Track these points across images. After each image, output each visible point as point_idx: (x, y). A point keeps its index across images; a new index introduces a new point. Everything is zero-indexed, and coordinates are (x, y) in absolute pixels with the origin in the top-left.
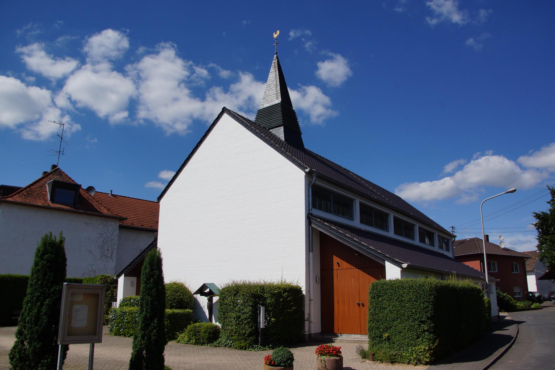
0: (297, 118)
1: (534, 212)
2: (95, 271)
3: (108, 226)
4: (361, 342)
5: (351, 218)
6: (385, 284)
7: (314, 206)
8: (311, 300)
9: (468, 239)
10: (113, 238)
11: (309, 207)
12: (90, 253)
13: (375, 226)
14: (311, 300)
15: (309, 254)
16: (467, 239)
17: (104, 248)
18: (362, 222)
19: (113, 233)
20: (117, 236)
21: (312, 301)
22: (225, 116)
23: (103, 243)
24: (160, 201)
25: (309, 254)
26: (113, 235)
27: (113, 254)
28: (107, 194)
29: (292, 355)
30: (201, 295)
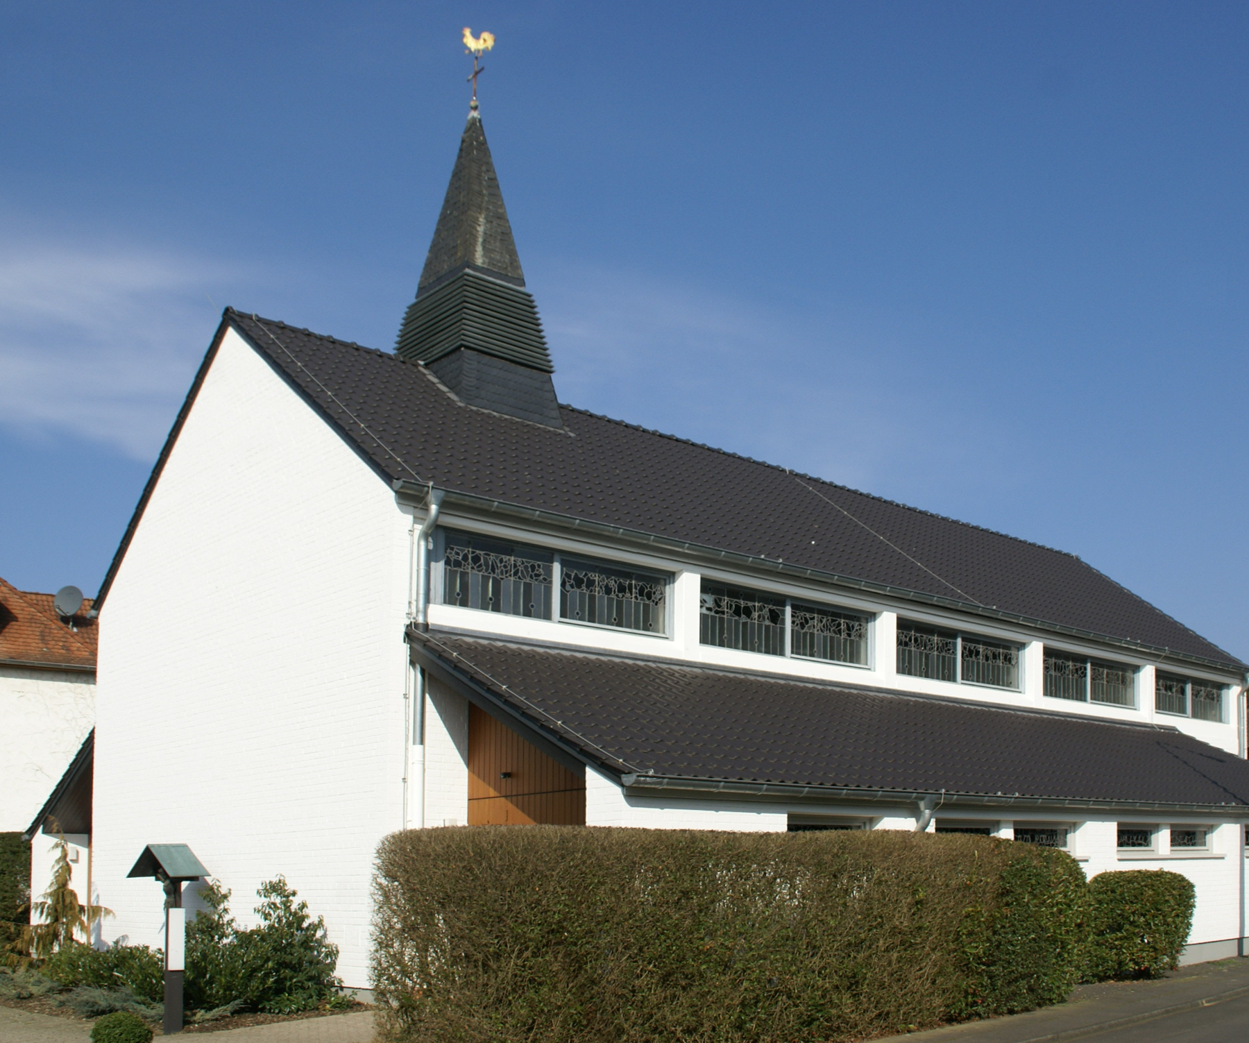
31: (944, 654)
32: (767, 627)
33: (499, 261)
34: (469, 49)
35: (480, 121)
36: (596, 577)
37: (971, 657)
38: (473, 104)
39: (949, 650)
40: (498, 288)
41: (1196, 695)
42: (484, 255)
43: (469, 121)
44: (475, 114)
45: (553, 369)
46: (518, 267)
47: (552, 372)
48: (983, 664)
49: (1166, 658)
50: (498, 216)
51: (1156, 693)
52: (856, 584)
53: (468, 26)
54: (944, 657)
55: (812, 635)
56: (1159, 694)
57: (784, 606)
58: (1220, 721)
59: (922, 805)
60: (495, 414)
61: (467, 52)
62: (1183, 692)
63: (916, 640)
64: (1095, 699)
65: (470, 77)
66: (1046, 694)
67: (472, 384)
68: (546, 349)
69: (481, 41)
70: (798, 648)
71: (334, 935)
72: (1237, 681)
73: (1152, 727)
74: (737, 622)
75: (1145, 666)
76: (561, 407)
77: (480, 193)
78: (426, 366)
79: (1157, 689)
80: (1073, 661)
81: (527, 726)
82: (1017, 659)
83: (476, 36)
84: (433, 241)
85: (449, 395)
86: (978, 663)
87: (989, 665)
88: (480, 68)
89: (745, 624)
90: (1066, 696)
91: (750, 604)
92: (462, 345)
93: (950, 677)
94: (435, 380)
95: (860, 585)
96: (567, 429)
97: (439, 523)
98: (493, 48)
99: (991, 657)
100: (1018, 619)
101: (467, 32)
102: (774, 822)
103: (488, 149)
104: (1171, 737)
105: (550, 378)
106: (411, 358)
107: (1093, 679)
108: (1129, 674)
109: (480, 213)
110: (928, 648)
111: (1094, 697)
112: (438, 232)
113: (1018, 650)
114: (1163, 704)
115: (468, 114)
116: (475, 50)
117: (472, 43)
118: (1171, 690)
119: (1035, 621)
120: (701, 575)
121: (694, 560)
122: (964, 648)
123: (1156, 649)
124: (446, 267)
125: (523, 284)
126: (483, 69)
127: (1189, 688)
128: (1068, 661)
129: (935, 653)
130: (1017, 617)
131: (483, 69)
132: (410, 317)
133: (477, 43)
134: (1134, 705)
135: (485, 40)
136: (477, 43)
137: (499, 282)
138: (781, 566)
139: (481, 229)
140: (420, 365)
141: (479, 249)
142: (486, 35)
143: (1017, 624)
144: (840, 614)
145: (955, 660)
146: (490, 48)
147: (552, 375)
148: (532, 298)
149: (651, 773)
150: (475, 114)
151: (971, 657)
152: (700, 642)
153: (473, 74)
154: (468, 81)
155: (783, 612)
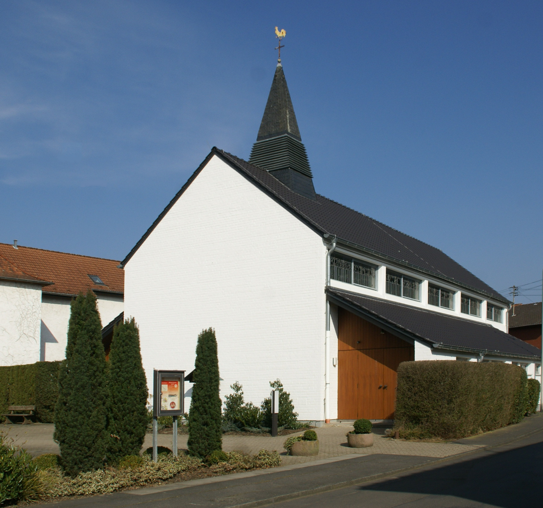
0: (307, 155)
1: (286, 389)
2: (13, 357)
3: (27, 294)
4: (341, 240)
5: (375, 288)
6: (414, 363)
7: (332, 277)
8: (327, 384)
9: (536, 303)
10: (34, 310)
11: (327, 279)
12: (4, 331)
13: (404, 295)
14: (327, 384)
15: (326, 332)
16: (534, 304)
17: (23, 325)
18: (388, 291)
19: (33, 303)
20: (40, 308)
21: (328, 385)
22: (215, 158)
23: (21, 317)
24: (124, 266)
25: (326, 332)
26: (34, 307)
27: (36, 332)
28: (10, 245)
29: (314, 432)
30: (190, 382)
31: (346, 269)
32: (398, 285)
34: (277, 36)
35: (282, 68)
36: (361, 267)
37: (357, 271)
39: (349, 267)
40: (296, 142)
41: (356, 270)
42: (290, 128)
43: (277, 67)
44: (279, 65)
45: (312, 176)
46: (299, 133)
47: (312, 177)
48: (362, 275)
49: (491, 298)
50: (292, 112)
51: (386, 282)
52: (410, 266)
53: (277, 26)
54: (347, 271)
55: (407, 288)
56: (388, 283)
57: (401, 278)
58: (501, 323)
59: (481, 354)
61: (277, 37)
62: (399, 282)
63: (336, 261)
64: (356, 283)
65: (277, 48)
66: (429, 303)
70: (464, 310)
71: (539, 381)
72: (506, 307)
73: (484, 324)
74: (391, 284)
75: (484, 300)
79: (387, 280)
80: (436, 289)
81: (379, 322)
82: (375, 273)
83: (280, 31)
84: (264, 117)
86: (360, 275)
87: (364, 276)
89: (393, 284)
90: (394, 294)
91: (394, 277)
93: (349, 282)
94: (272, 176)
95: (411, 266)
97: (335, 250)
98: (286, 36)
99: (365, 272)
100: (417, 268)
101: (277, 28)
102: (454, 358)
103: (286, 81)
104: (491, 328)
106: (261, 166)
107: (471, 305)
108: (417, 284)
110: (340, 266)
111: (356, 282)
113: (501, 310)
114: (390, 290)
115: (277, 65)
117: (277, 32)
118: (393, 281)
119: (385, 256)
120: (386, 267)
121: (461, 287)
122: (354, 267)
123: (382, 255)
124: (274, 130)
125: (301, 140)
126: (284, 46)
127: (493, 309)
128: (434, 288)
129: (343, 268)
130: (417, 267)
131: (284, 46)
133: (281, 34)
134: (453, 309)
136: (281, 34)
137: (295, 139)
138: (407, 264)
139: (288, 116)
141: (288, 125)
142: (283, 30)
143: (417, 270)
144: (368, 266)
145: (439, 298)
146: (284, 36)
147: (312, 179)
148: (304, 146)
149: (442, 343)
151: (357, 271)
152: (386, 292)
153: (278, 47)
154: (275, 49)
155: (401, 279)
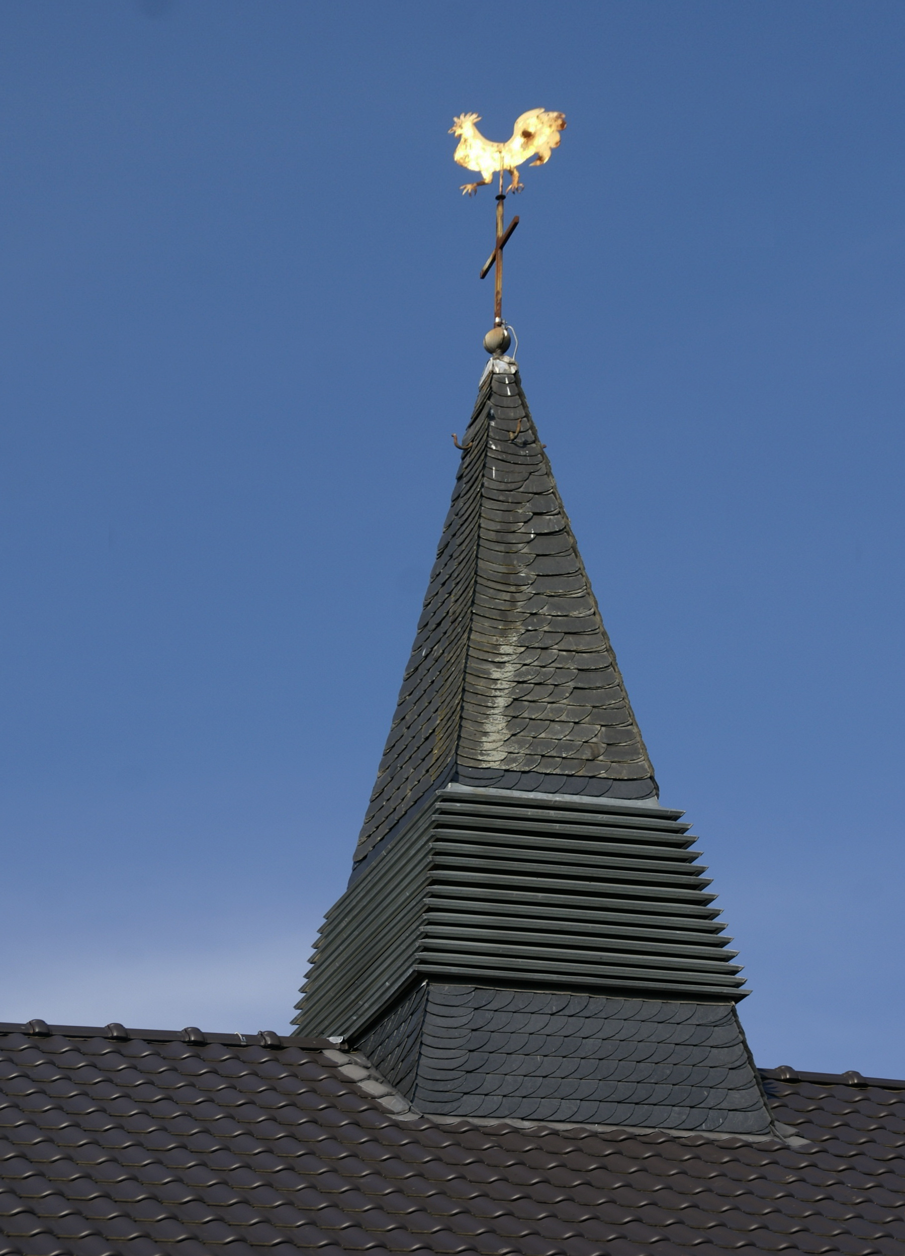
33: (568, 747)
38: (491, 337)
44: (501, 365)
45: (742, 990)
47: (739, 998)
60: (527, 1124)
67: (454, 1064)
68: (723, 944)
69: (517, 140)
76: (764, 1078)
77: (509, 580)
78: (351, 1045)
85: (385, 1102)
88: (509, 223)
92: (419, 976)
96: (783, 1129)
105: (734, 1011)
109: (504, 633)
112: (400, 718)
116: (496, 175)
132: (327, 936)
135: (527, 135)
139: (504, 675)
140: (332, 1046)
142: (530, 120)
147: (740, 1007)
150: (501, 365)
